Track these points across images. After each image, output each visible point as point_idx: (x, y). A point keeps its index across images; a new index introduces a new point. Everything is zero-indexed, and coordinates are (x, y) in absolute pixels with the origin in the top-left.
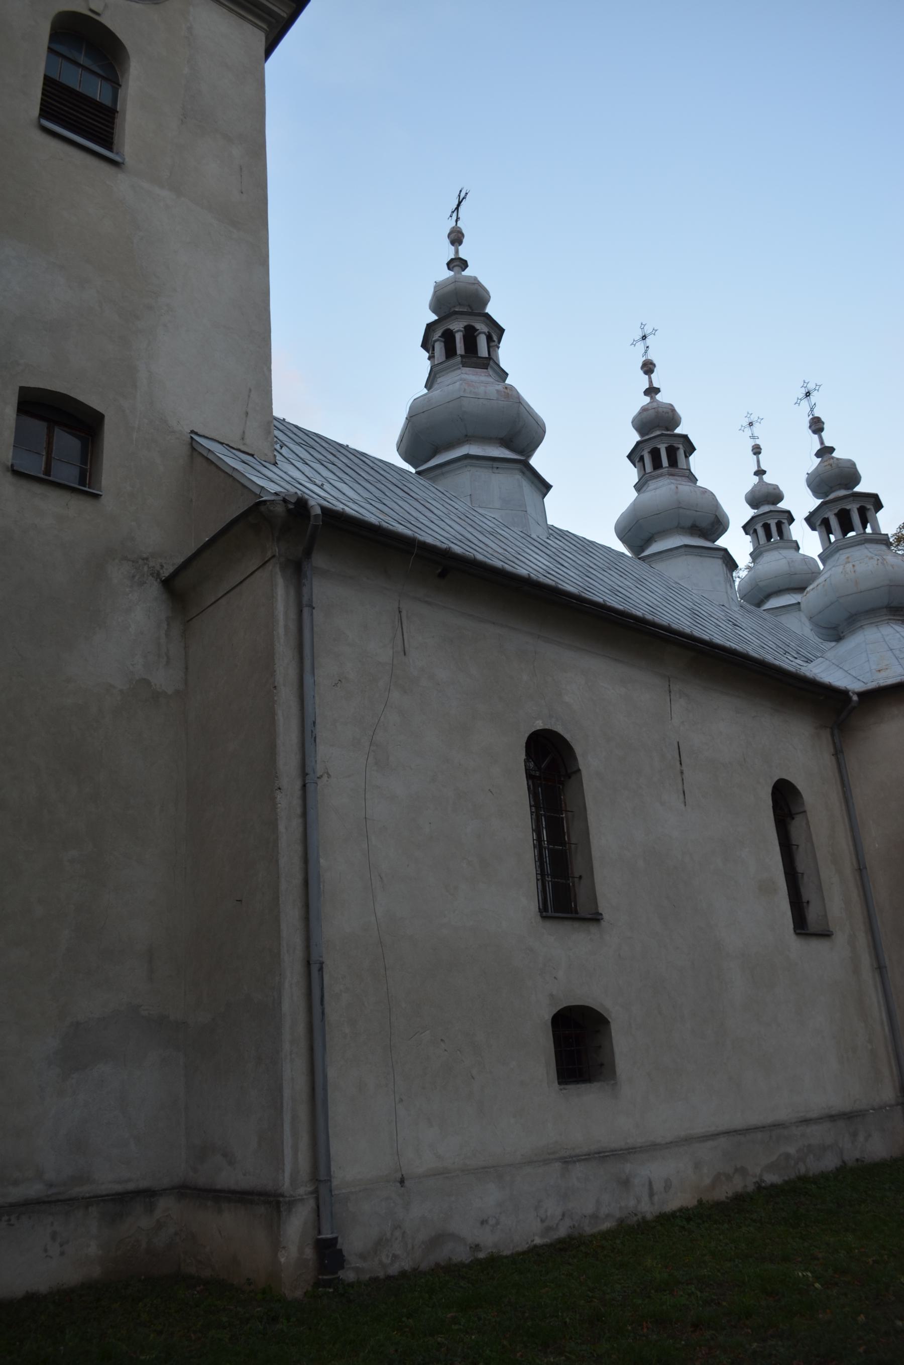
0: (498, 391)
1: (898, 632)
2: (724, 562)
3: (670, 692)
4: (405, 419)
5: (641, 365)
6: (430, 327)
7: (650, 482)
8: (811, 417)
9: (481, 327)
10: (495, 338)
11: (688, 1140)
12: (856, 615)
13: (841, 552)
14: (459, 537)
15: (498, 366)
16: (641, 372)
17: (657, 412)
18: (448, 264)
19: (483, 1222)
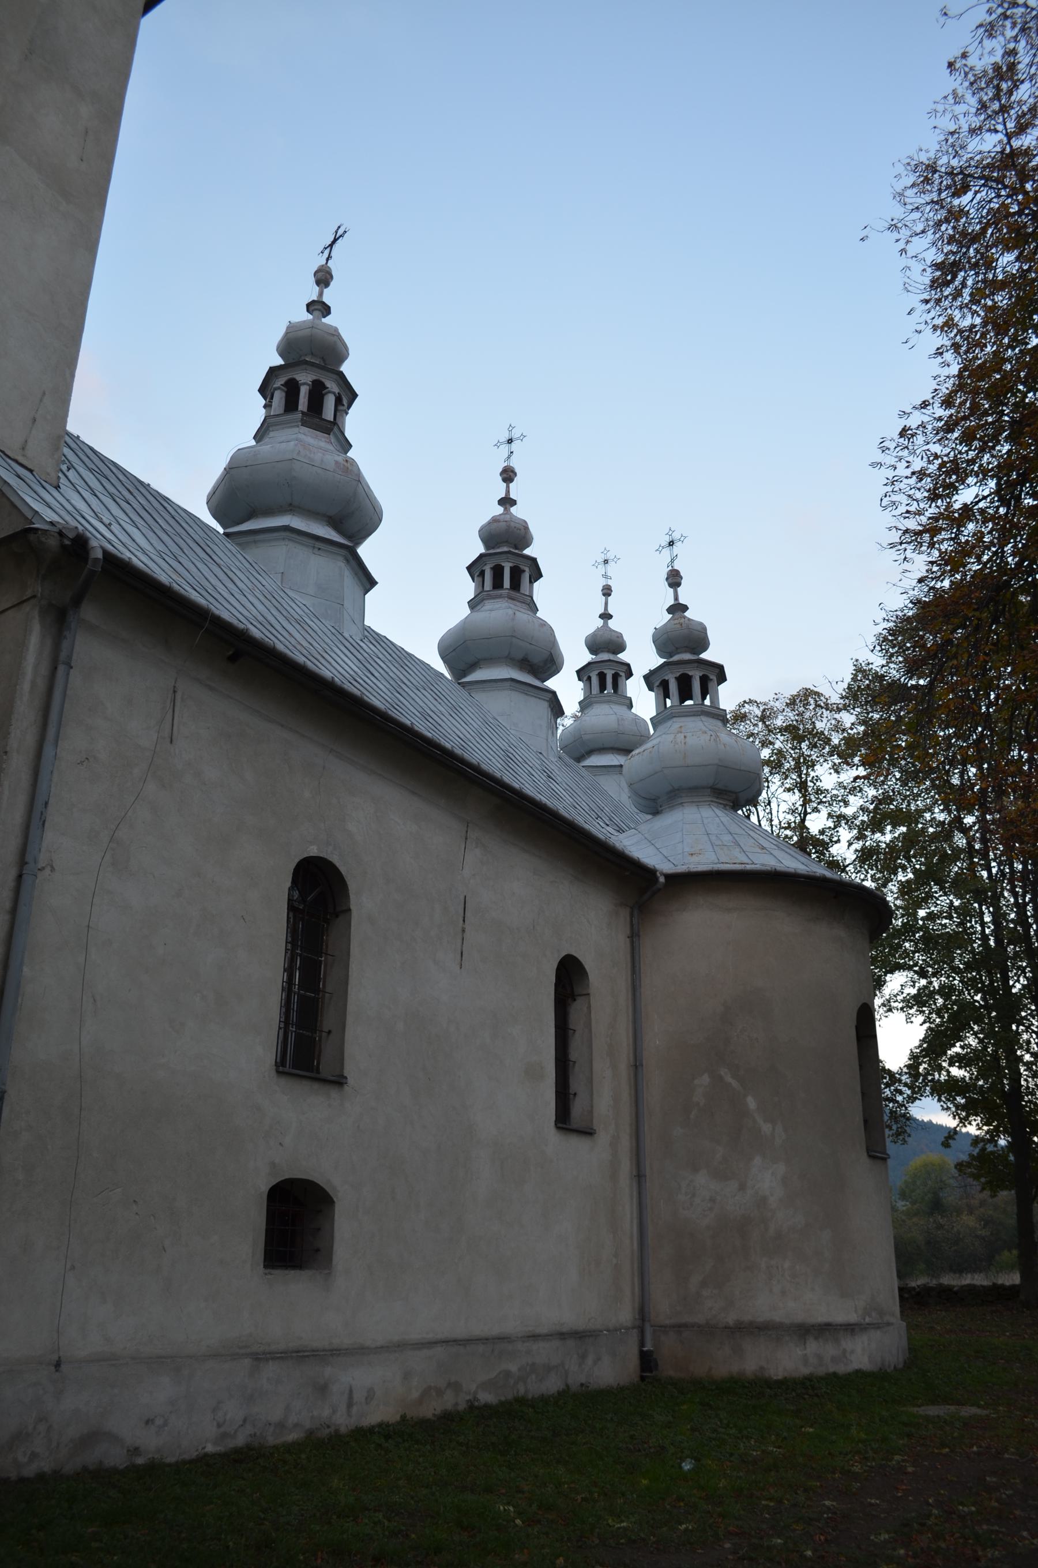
0: (337, 462)
2: (550, 706)
3: (466, 839)
6: (273, 372)
8: (670, 568)
9: (331, 385)
10: (345, 402)
11: (401, 1346)
12: (678, 790)
13: (675, 719)
14: (260, 618)
15: (343, 434)
16: (500, 478)
17: (509, 527)
18: (308, 306)
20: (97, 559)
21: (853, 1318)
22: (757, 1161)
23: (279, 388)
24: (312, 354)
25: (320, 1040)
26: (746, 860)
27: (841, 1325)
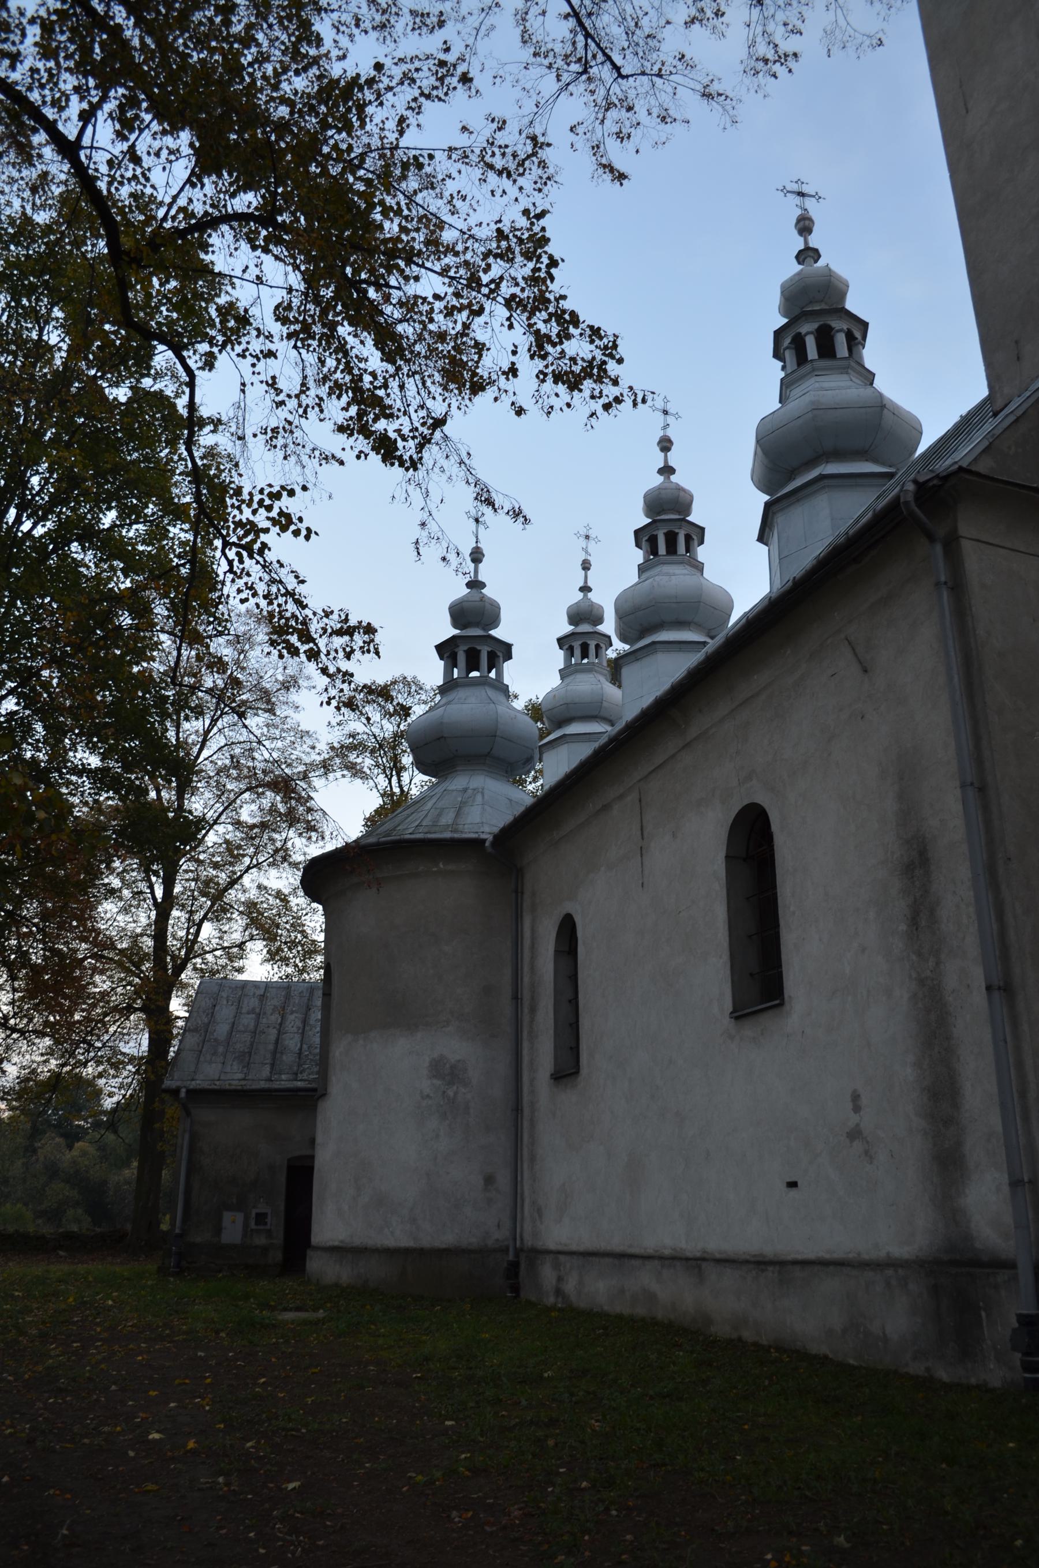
6: (778, 334)
9: (837, 324)
10: (858, 335)
15: (863, 367)
16: (658, 449)
18: (797, 257)
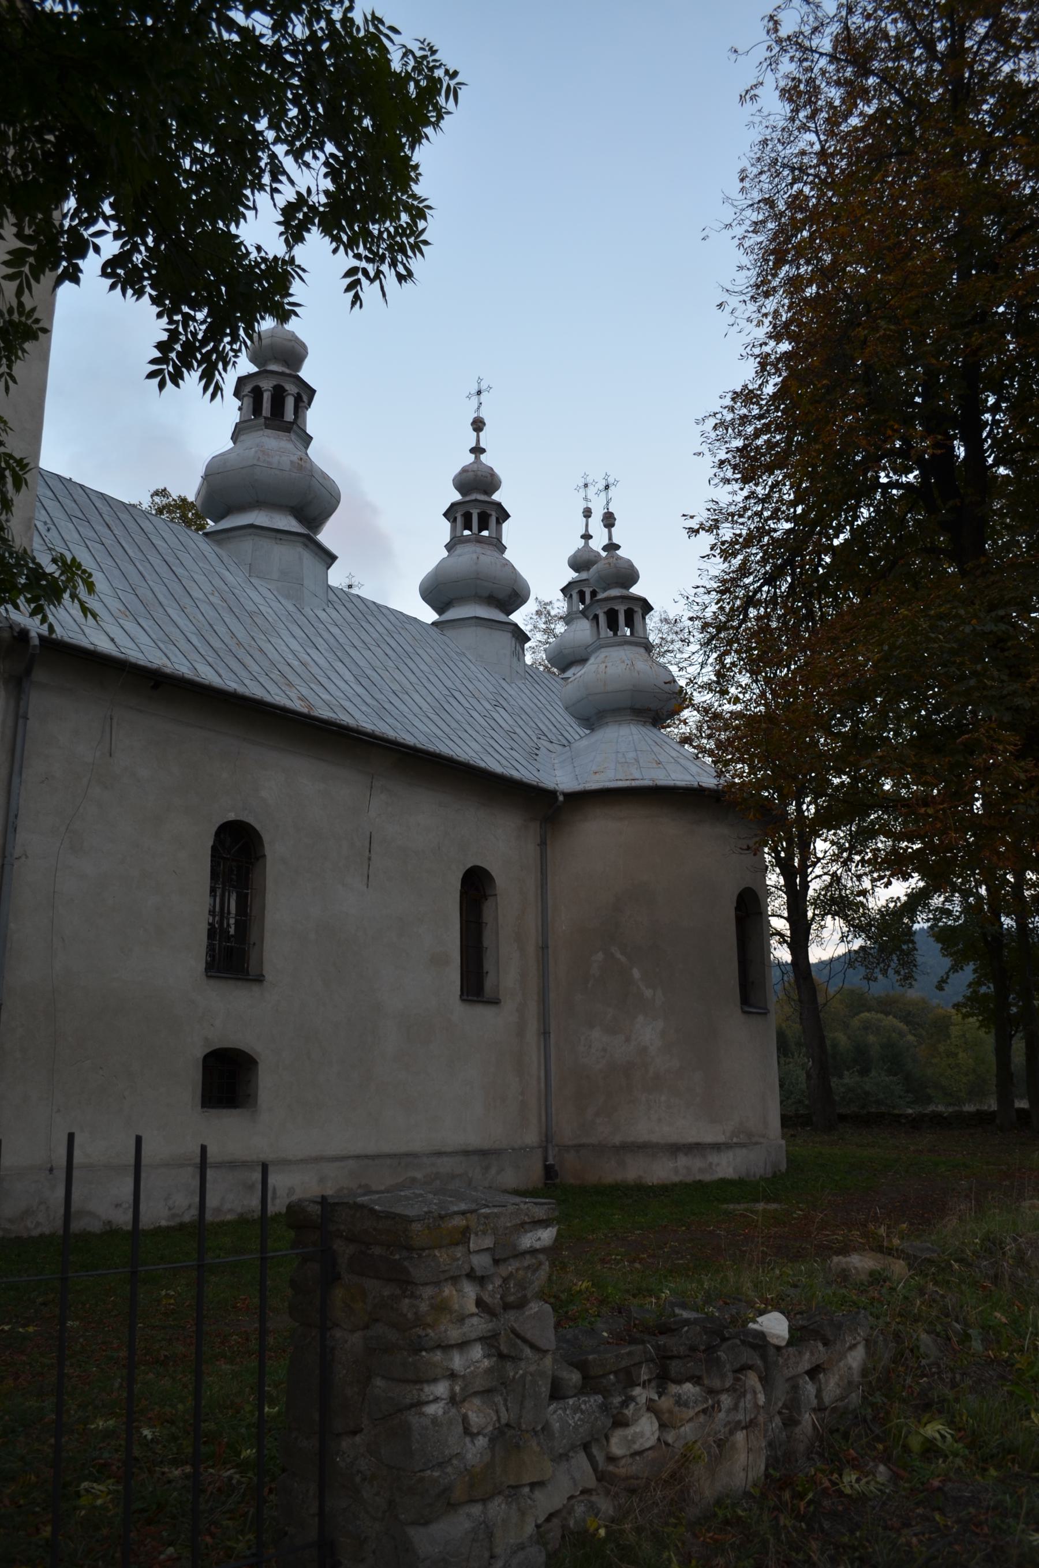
0: (292, 462)
1: (632, 734)
2: (513, 636)
3: (372, 787)
4: (200, 480)
5: (471, 421)
7: (458, 546)
8: (606, 510)
9: (291, 388)
10: (305, 398)
11: (318, 1160)
13: (603, 650)
16: (471, 428)
17: (476, 476)
19: (117, 1206)
20: (35, 646)
21: (721, 1139)
22: (641, 1018)
23: (247, 395)
24: (275, 358)
25: (249, 948)
26: (637, 775)
27: (709, 1144)
